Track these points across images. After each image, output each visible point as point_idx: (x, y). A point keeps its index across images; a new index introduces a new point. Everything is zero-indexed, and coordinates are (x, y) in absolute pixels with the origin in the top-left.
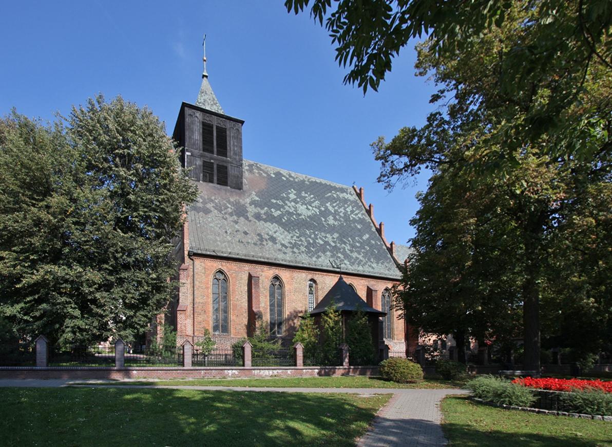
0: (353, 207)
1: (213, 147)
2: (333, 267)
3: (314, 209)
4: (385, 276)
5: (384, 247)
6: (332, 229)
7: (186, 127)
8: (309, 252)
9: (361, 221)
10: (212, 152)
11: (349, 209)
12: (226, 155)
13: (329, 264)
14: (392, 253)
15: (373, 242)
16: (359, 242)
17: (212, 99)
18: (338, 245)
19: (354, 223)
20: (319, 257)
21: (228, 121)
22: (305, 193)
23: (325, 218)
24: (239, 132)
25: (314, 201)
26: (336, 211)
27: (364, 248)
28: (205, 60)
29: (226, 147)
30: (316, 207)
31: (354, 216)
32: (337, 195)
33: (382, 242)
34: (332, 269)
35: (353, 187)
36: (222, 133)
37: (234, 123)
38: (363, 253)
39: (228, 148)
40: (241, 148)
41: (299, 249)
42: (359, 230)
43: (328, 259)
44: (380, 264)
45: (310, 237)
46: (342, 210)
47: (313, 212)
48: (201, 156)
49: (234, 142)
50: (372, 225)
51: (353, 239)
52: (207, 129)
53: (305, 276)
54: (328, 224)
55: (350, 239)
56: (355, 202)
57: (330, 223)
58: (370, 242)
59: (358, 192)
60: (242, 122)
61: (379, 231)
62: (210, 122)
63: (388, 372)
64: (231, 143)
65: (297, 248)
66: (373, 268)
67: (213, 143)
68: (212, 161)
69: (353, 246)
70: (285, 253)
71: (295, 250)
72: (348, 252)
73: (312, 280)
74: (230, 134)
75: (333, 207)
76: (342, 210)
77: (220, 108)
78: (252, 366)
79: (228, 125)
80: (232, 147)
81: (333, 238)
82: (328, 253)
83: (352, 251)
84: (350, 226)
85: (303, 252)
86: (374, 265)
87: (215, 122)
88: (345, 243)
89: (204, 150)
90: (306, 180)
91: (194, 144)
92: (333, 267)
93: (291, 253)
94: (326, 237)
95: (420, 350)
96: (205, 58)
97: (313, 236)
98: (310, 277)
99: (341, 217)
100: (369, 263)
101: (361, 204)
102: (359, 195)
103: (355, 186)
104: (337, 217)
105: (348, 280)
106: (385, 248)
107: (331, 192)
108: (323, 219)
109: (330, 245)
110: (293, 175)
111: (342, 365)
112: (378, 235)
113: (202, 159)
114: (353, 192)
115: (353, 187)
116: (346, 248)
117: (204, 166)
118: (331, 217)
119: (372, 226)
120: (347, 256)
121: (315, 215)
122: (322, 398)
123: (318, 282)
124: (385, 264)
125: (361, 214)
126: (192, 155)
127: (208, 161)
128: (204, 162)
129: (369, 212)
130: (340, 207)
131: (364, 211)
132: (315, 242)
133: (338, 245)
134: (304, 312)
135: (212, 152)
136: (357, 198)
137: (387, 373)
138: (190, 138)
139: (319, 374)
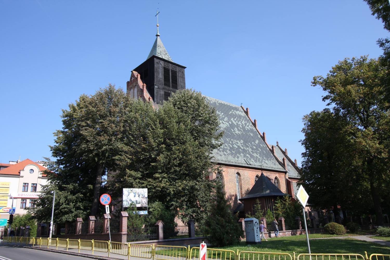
0: (245, 121)
1: (170, 83)
2: (248, 164)
3: (226, 123)
4: (275, 169)
5: (268, 149)
6: (239, 137)
7: (155, 70)
8: (232, 154)
9: (252, 131)
10: (169, 86)
11: (243, 122)
12: (177, 88)
13: (245, 162)
14: (274, 153)
15: (262, 145)
16: (254, 146)
17: (164, 51)
18: (245, 148)
19: (248, 132)
20: (238, 157)
21: (177, 67)
22: (219, 112)
23: (233, 129)
24: (183, 73)
25: (225, 117)
26: (237, 124)
27: (258, 150)
28: (158, 26)
29: (177, 83)
30: (227, 122)
31: (247, 128)
32: (235, 112)
33: (266, 145)
34: (247, 165)
35: (241, 106)
36: (174, 73)
37: (181, 68)
38: (259, 153)
39: (178, 84)
40: (185, 83)
41: (227, 152)
42: (252, 137)
43: (243, 159)
44: (269, 161)
45: (230, 143)
46: (240, 123)
47: (226, 125)
48: (163, 89)
49: (181, 80)
50: (258, 133)
51: (251, 143)
52: (166, 71)
53: (233, 171)
54: (236, 134)
55: (249, 144)
56: (244, 117)
57: (236, 132)
58: (260, 146)
59: (246, 110)
60: (185, 68)
61: (263, 138)
62: (168, 68)
63: (332, 230)
64: (179, 80)
65: (226, 151)
66: (267, 164)
67: (169, 81)
68: (169, 92)
69: (253, 149)
70: (221, 155)
71: (225, 153)
72: (251, 153)
73: (238, 174)
74: (179, 75)
75: (235, 121)
76: (240, 123)
77: (169, 56)
78: (286, 230)
79: (178, 69)
80: (180, 83)
81: (241, 143)
82: (242, 154)
83: (253, 153)
84: (247, 135)
85: (229, 154)
86: (267, 162)
87: (170, 67)
88: (248, 147)
89: (165, 85)
90: (216, 102)
91: (159, 81)
92: (248, 164)
93: (224, 155)
94: (237, 143)
95: (326, 219)
96: (158, 25)
97: (231, 142)
98: (237, 171)
99: (241, 128)
100: (264, 160)
101: (248, 119)
102: (246, 113)
103: (243, 106)
104: (239, 128)
105: (266, 174)
106: (269, 149)
107: (231, 111)
108: (233, 130)
109: (241, 148)
110: (209, 99)
111: (299, 229)
112: (262, 140)
113: (164, 90)
114: (242, 110)
115: (241, 106)
116: (250, 150)
117: (165, 95)
118: (236, 129)
119: (258, 134)
120: (252, 156)
121: (228, 127)
122: (353, 234)
123: (241, 174)
124: (272, 160)
125: (250, 126)
126: (158, 88)
127: (167, 92)
128: (165, 92)
129: (254, 124)
130: (238, 121)
131: (251, 124)
132: (233, 146)
133: (245, 148)
134: (235, 195)
135: (169, 86)
136: (245, 114)
137: (331, 231)
138: (157, 77)
139: (291, 234)
